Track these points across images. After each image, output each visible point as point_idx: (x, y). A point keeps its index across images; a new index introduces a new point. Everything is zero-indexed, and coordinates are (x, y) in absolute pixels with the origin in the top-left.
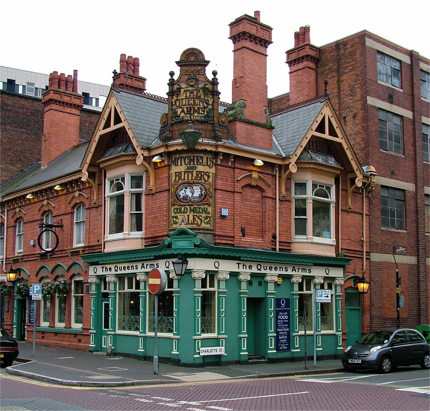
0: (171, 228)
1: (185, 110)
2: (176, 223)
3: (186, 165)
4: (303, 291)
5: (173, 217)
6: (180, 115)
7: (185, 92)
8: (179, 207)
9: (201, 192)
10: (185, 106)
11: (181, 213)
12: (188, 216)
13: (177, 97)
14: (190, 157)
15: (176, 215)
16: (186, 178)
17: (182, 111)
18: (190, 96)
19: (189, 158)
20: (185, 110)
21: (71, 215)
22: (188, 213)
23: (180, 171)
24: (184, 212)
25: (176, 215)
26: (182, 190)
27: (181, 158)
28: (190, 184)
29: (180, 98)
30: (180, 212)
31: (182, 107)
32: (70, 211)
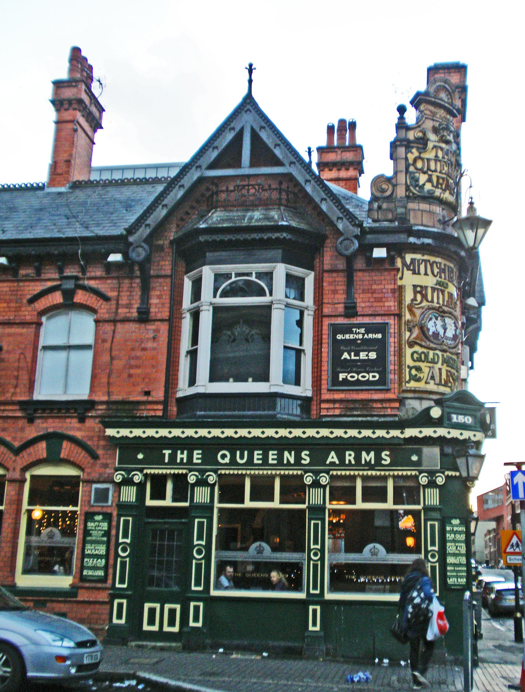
0: (404, 388)
1: (435, 179)
2: (419, 380)
3: (435, 276)
4: (354, 503)
5: (411, 368)
6: (424, 185)
7: (435, 149)
8: (425, 351)
9: (456, 331)
10: (434, 173)
11: (427, 362)
12: (440, 369)
13: (420, 153)
14: (440, 263)
15: (418, 364)
16: (435, 300)
17: (430, 180)
18: (443, 158)
19: (438, 265)
20: (435, 179)
21: (36, 328)
22: (439, 365)
23: (423, 284)
24: (433, 362)
25: (418, 364)
26: (431, 319)
27: (425, 261)
28: (441, 312)
29: (425, 155)
30: (426, 360)
31: (430, 173)
32: (35, 319)
